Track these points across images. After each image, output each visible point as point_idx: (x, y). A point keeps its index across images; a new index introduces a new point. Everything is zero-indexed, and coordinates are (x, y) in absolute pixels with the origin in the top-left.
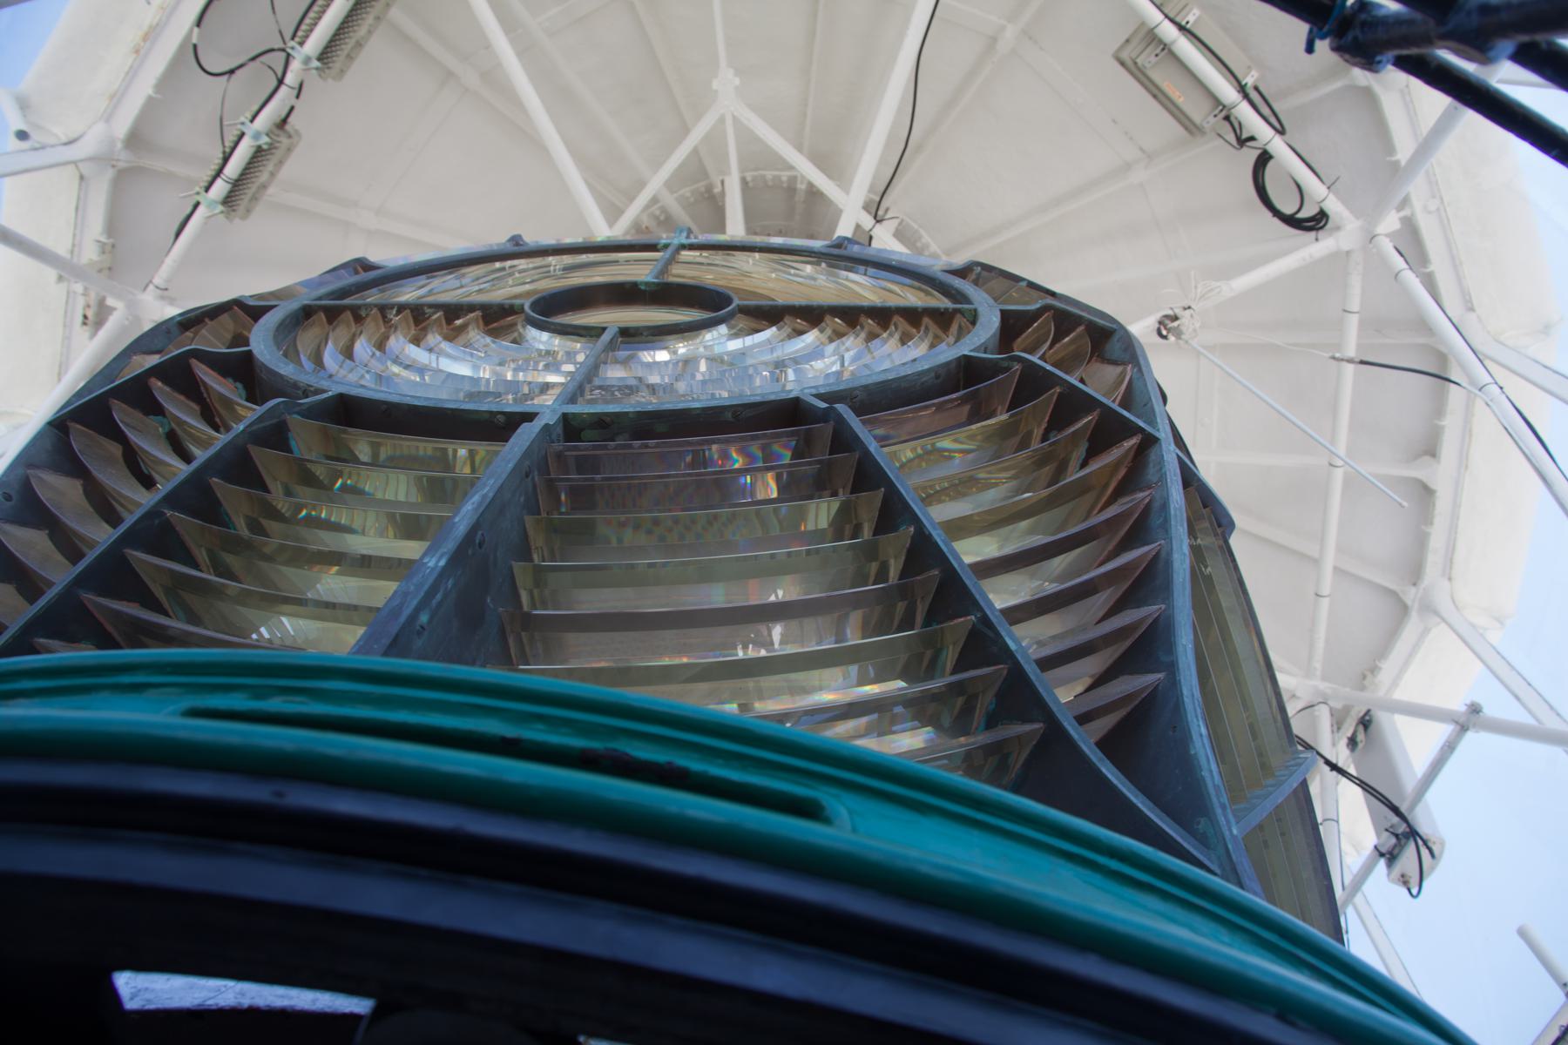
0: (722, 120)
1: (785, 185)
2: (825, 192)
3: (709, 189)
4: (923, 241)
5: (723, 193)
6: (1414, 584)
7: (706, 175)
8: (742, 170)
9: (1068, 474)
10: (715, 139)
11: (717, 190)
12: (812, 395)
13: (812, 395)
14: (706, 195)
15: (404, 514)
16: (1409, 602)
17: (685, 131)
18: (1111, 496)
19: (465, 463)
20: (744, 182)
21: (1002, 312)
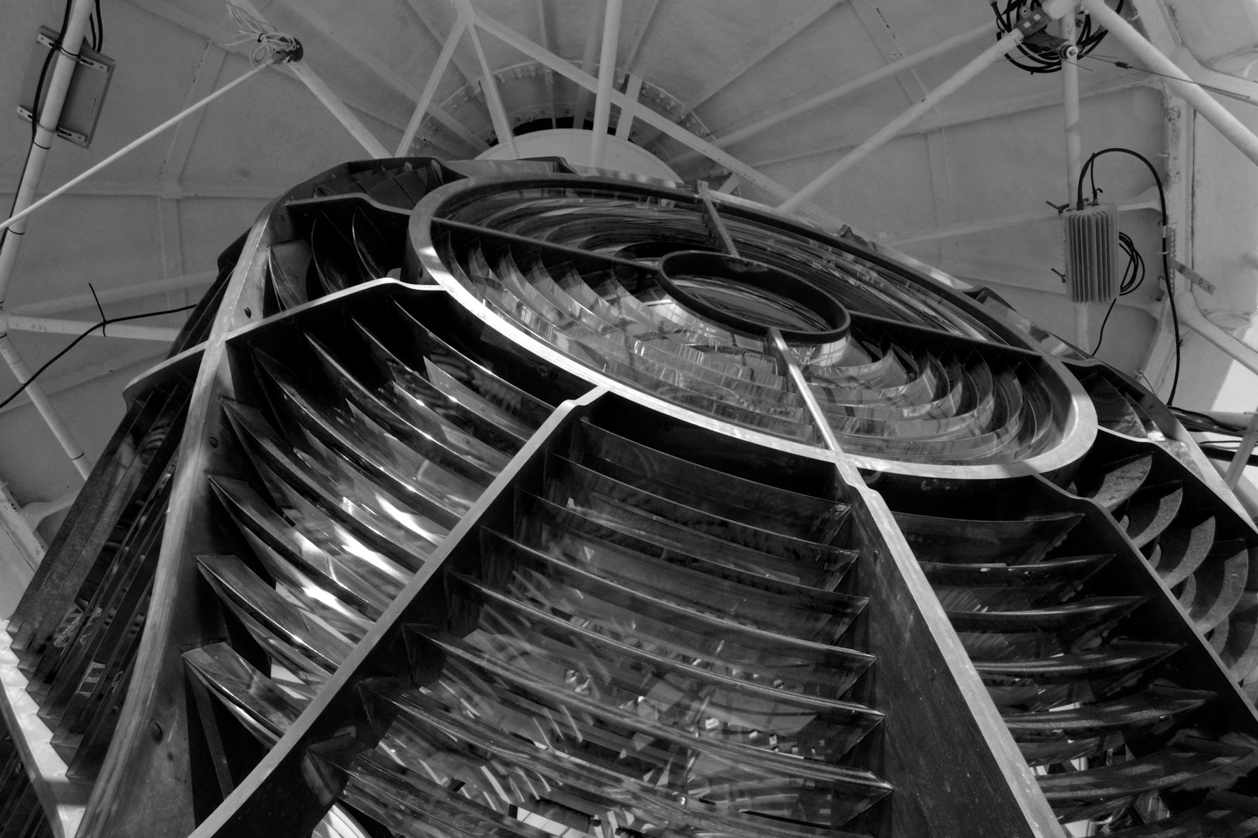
0: (467, 29)
1: (533, 74)
2: (653, 124)
3: (469, 90)
4: (662, 96)
5: (482, 93)
6: (1159, 300)
7: (464, 81)
8: (492, 68)
9: (534, 235)
10: (464, 48)
11: (477, 91)
12: (966, 293)
13: (966, 293)
14: (466, 99)
15: (859, 318)
16: (1158, 317)
17: (439, 48)
18: (271, 280)
19: (163, 483)
20: (497, 79)
21: (1099, 431)
